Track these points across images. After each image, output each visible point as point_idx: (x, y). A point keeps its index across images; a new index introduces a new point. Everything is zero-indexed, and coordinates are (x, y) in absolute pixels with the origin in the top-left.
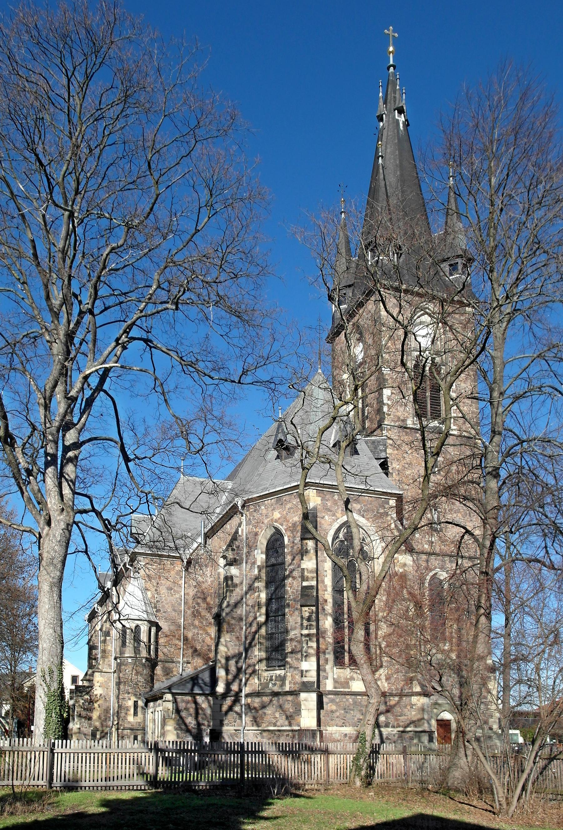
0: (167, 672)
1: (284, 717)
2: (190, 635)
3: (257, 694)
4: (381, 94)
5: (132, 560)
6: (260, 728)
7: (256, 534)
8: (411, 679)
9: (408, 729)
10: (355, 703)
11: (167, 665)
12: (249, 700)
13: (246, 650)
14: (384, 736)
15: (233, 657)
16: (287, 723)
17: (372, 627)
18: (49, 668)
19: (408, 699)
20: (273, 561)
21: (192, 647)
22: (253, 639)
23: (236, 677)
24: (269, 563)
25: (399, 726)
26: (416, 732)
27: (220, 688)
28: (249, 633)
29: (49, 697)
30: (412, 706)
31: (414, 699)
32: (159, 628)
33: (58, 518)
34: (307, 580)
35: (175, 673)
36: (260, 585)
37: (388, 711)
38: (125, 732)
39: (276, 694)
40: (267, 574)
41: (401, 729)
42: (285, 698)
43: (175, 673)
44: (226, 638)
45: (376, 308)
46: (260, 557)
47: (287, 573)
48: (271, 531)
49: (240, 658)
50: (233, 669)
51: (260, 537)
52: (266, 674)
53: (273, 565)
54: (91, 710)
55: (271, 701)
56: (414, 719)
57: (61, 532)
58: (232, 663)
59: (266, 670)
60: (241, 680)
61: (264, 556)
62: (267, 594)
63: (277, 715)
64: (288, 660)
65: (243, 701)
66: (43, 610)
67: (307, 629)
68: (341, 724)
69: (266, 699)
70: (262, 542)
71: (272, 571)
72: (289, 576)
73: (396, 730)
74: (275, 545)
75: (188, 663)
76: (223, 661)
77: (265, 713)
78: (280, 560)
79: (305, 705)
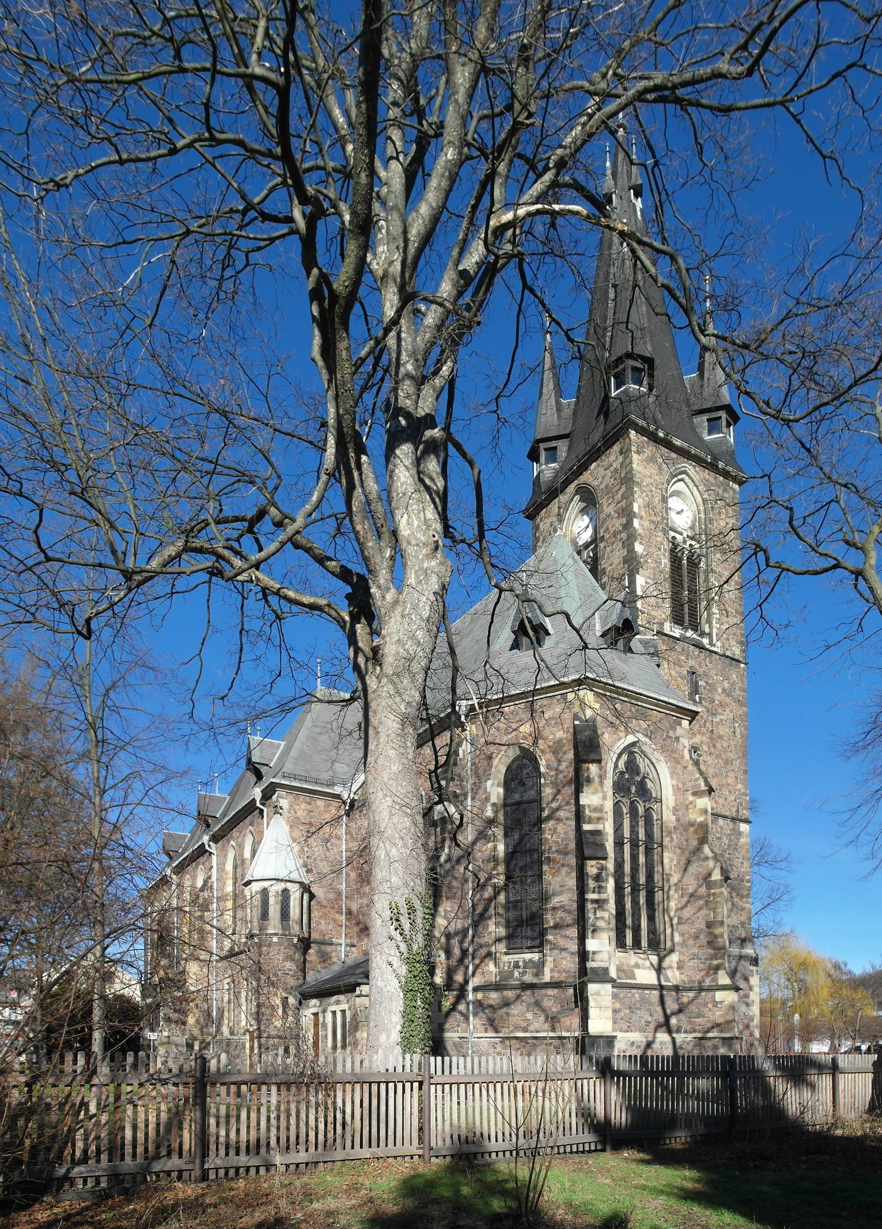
0: (325, 958)
1: (542, 1018)
2: (354, 907)
3: (497, 987)
4: (608, 164)
5: (267, 795)
6: (500, 1035)
7: (490, 758)
8: (717, 968)
9: (710, 1035)
10: (642, 999)
11: (323, 947)
12: (480, 995)
13: (475, 925)
14: (678, 1044)
15: (456, 934)
16: (546, 1026)
17: (658, 896)
18: (408, 902)
19: (710, 994)
20: (517, 797)
21: (358, 924)
22: (486, 909)
23: (461, 961)
24: (509, 801)
25: (695, 1031)
26: (724, 1039)
27: (439, 979)
28: (479, 900)
29: (408, 961)
30: (715, 1004)
31: (719, 995)
32: (312, 896)
33: (426, 565)
34: (589, 823)
35: (335, 960)
36: (499, 832)
37: (680, 1011)
38: (271, 1042)
39: (532, 987)
40: (506, 814)
41: (699, 1035)
42: (544, 991)
43: (335, 960)
44: (446, 906)
45: (625, 458)
46: (495, 791)
47: (545, 814)
48: (513, 753)
49: (465, 936)
50: (457, 952)
51: (495, 762)
52: (506, 958)
53: (519, 803)
54: (184, 1013)
55: (518, 997)
56: (721, 1020)
57: (433, 598)
58: (455, 942)
59: (506, 954)
60: (467, 968)
61: (501, 790)
62: (507, 845)
63: (530, 1016)
64: (550, 937)
65: (471, 997)
66: (386, 776)
67: (594, 892)
68: (625, 1028)
69: (510, 994)
70: (500, 766)
71: (514, 812)
72: (549, 818)
73: (690, 1037)
74: (522, 772)
75: (353, 946)
76: (443, 940)
77: (508, 1014)
78: (532, 793)
79: (595, 1000)
